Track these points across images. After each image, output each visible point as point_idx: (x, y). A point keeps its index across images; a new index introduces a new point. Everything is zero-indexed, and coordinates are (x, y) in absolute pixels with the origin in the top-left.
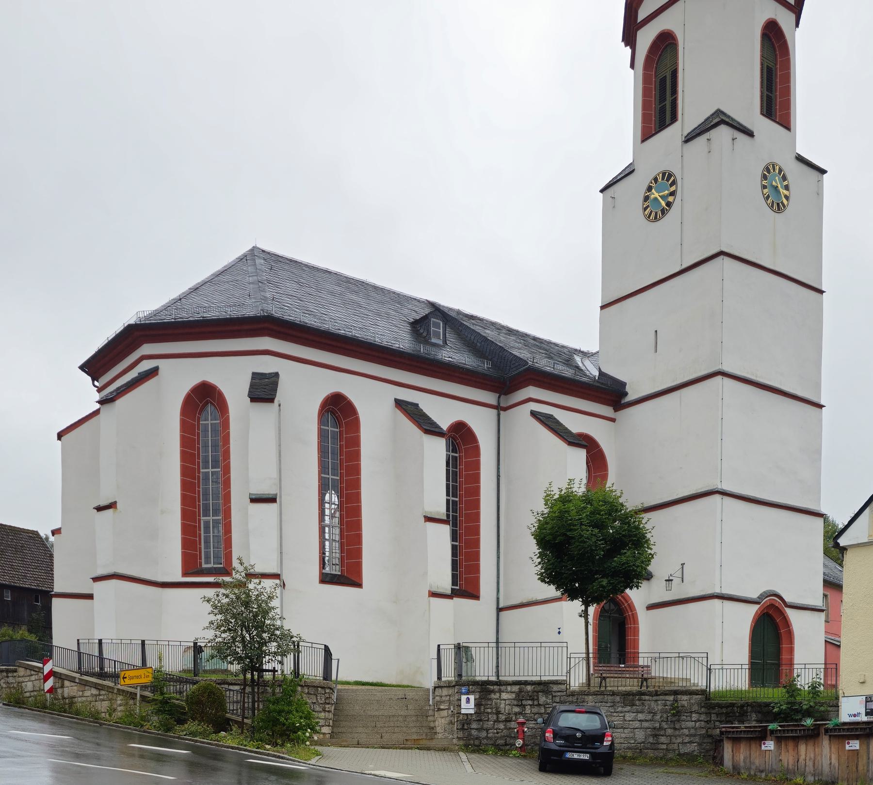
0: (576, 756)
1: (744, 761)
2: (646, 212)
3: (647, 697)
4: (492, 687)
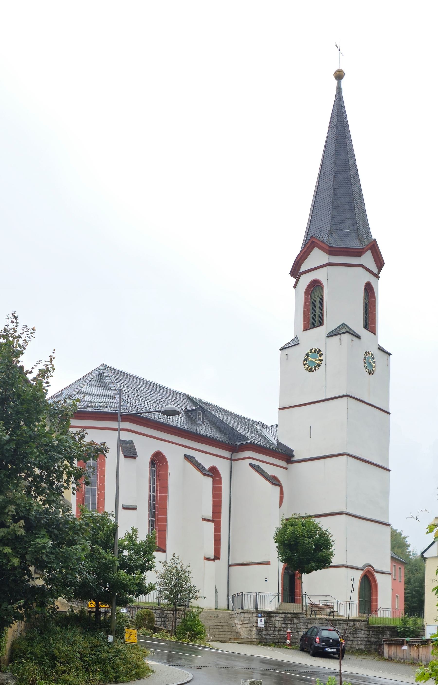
0: (330, 650)
1: (394, 654)
2: (306, 366)
3: (342, 622)
4: (272, 615)
